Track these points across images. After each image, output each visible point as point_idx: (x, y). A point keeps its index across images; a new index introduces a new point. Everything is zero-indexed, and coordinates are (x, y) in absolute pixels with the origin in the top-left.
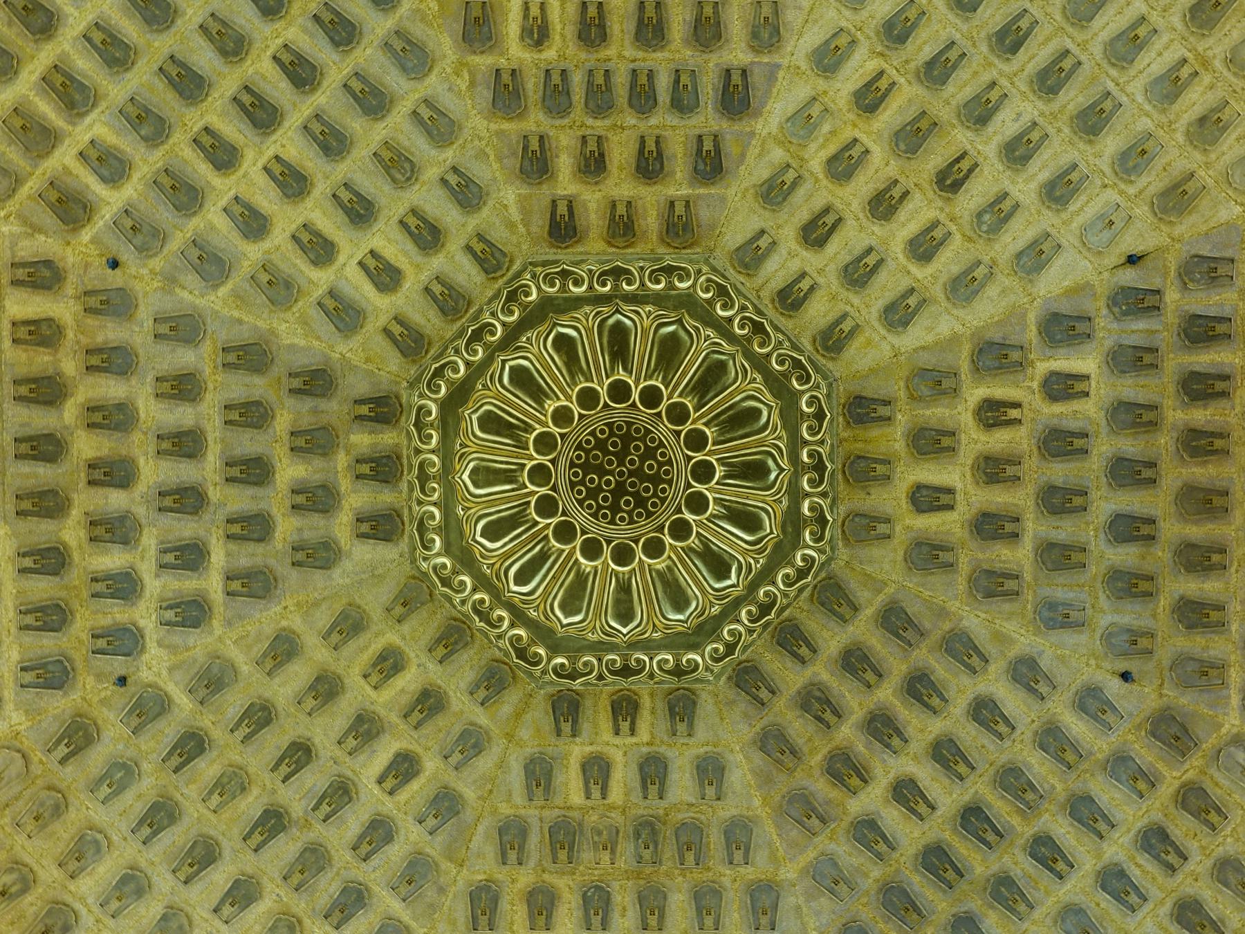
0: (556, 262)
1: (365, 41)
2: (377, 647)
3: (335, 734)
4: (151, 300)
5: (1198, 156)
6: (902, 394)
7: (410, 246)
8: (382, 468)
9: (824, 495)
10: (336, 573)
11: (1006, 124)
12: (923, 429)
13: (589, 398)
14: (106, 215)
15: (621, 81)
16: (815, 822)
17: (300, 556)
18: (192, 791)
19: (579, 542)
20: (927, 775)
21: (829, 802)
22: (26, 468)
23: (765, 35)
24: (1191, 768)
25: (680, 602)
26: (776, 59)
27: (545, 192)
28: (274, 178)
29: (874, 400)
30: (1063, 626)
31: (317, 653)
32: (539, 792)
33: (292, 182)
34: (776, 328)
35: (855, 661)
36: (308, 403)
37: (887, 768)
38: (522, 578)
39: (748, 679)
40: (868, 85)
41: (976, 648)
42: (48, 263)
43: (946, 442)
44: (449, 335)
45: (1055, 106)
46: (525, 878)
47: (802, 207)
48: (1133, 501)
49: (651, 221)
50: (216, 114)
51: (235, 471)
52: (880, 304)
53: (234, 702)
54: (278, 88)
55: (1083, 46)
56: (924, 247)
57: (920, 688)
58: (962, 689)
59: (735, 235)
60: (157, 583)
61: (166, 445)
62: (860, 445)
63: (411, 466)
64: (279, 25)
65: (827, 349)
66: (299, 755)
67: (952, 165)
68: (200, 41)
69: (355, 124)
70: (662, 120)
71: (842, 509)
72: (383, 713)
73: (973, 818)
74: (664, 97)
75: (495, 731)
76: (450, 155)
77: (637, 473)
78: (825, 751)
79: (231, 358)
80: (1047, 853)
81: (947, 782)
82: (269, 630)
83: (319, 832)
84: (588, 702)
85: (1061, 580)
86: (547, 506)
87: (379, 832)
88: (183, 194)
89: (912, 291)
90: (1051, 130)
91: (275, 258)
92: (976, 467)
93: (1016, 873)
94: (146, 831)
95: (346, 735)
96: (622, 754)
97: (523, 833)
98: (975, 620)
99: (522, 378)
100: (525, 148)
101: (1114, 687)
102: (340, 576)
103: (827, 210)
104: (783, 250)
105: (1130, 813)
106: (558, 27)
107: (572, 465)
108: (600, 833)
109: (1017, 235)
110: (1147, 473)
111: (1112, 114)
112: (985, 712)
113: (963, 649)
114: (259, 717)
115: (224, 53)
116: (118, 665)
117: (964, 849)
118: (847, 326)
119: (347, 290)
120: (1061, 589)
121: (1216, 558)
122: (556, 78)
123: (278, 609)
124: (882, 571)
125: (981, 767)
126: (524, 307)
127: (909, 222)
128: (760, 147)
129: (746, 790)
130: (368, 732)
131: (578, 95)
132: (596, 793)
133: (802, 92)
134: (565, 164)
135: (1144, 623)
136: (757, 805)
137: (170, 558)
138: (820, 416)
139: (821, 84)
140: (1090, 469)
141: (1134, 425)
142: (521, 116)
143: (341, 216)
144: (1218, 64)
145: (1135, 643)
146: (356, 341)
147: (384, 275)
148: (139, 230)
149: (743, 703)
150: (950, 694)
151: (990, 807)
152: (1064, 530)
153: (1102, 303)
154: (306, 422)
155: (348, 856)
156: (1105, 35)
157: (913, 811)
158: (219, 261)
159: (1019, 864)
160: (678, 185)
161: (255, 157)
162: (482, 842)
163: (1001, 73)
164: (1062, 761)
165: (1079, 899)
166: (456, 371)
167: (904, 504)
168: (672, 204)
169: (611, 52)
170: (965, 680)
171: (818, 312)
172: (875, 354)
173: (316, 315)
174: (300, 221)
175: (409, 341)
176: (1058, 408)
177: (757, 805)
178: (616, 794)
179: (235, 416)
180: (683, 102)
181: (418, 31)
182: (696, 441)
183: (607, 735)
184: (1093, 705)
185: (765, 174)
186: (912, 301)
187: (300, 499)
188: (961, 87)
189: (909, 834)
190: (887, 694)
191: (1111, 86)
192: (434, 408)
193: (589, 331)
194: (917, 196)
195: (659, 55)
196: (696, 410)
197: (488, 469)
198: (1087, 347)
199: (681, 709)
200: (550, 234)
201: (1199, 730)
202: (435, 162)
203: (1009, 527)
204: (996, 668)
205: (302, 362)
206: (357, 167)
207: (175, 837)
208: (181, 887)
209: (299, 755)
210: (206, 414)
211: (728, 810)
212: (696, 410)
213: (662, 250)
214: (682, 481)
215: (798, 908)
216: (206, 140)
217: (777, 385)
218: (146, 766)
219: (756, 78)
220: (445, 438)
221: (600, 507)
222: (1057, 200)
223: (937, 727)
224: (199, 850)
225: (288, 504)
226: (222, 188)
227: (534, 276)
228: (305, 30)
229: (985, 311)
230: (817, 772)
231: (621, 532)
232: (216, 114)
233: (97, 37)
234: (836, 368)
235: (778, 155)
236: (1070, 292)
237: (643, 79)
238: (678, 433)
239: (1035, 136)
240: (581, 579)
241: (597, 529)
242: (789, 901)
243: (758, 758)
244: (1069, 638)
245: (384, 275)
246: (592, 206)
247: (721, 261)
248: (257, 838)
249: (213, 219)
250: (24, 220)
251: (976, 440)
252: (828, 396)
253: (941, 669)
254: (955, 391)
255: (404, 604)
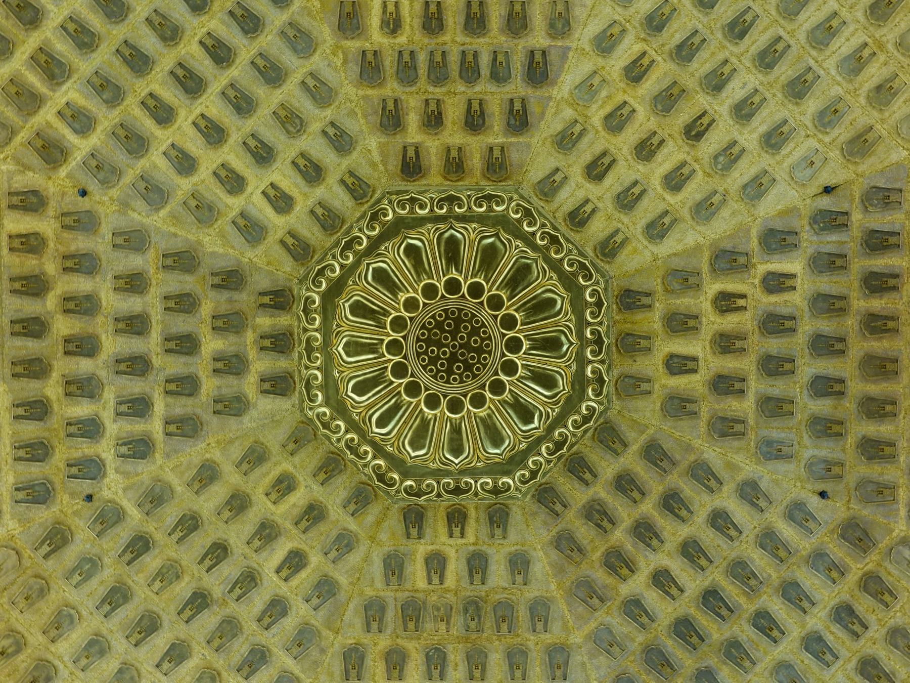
0: (406, 191)
1: (267, 30)
2: (275, 473)
3: (245, 537)
4: (110, 219)
5: (875, 114)
6: (659, 288)
7: (300, 180)
8: (279, 343)
9: (602, 362)
10: (246, 419)
11: (735, 91)
12: (674, 314)
13: (430, 291)
14: (77, 158)
15: (454, 59)
16: (595, 601)
17: (219, 407)
18: (141, 579)
19: (423, 396)
20: (677, 567)
21: (606, 587)
22: (19, 342)
23: (559, 26)
24: (870, 562)
25: (497, 440)
26: (567, 43)
27: (399, 140)
28: (200, 130)
29: (639, 293)
30: (777, 458)
31: (232, 478)
32: (394, 579)
33: (213, 133)
34: (568, 240)
35: (625, 484)
36: (225, 295)
37: (648, 562)
38: (381, 423)
39: (546, 496)
40: (634, 62)
41: (713, 474)
42: (35, 193)
43: (691, 323)
44: (328, 245)
45: (771, 77)
46: (384, 642)
47: (586, 151)
48: (828, 367)
49: (476, 162)
50: (158, 83)
51: (172, 345)
52: (643, 222)
53: (171, 514)
54: (203, 64)
55: (792, 33)
56: (675, 181)
57: (672, 503)
58: (703, 504)
59: (537, 172)
60: (115, 426)
61: (121, 326)
62: (628, 326)
63: (300, 341)
64: (204, 18)
65: (604, 255)
66: (219, 552)
67: (696, 120)
68: (146, 30)
69: (260, 91)
70: (484, 88)
71: (616, 372)
72: (280, 521)
73: (711, 598)
74: (485, 71)
75: (362, 534)
76: (329, 113)
77: (466, 346)
78: (603, 549)
79: (169, 262)
80: (765, 624)
81: (692, 572)
82: (197, 461)
83: (233, 608)
84: (430, 513)
85: (775, 424)
86: (400, 370)
87: (277, 609)
88: (134, 142)
89: (666, 212)
90: (768, 95)
91: (201, 189)
92: (713, 342)
93: (743, 638)
94: (107, 608)
95: (253, 537)
96: (455, 551)
97: (383, 609)
98: (713, 453)
99: (381, 277)
100: (384, 108)
101: (814, 502)
102: (248, 421)
103: (604, 154)
104: (572, 183)
105: (826, 594)
106: (408, 20)
107: (418, 340)
108: (438, 609)
109: (744, 172)
110: (838, 346)
111: (813, 83)
112: (720, 521)
113: (704, 475)
114: (190, 524)
115: (164, 39)
116: (86, 486)
117: (704, 621)
118: (619, 238)
119: (253, 212)
120: (776, 431)
121: (888, 408)
122: (406, 57)
123: (203, 445)
124: (645, 417)
125: (717, 561)
126: (383, 224)
127: (664, 162)
128: (556, 108)
129: (545, 578)
130: (269, 535)
131: (423, 69)
132: (436, 580)
133: (586, 67)
134: (413, 120)
135: (836, 455)
136: (553, 589)
137: (124, 408)
138: (599, 304)
139: (600, 61)
140: (797, 343)
141: (829, 311)
142: (381, 85)
143: (249, 158)
144: (890, 47)
145: (829, 470)
146: (261, 249)
147: (281, 201)
148: (101, 169)
149: (543, 514)
150: (695, 508)
151: (723, 590)
152: (778, 388)
153: (805, 222)
154: (224, 309)
155: (254, 626)
156: (808, 26)
157: (667, 593)
158: (160, 191)
159: (745, 632)
160: (496, 136)
161: (187, 115)
162: (353, 616)
163: (732, 54)
164: (776, 556)
165: (789, 657)
166: (333, 271)
167: (661, 368)
168: (491, 149)
169: (447, 38)
170: (706, 497)
171: (598, 228)
172: (639, 259)
173: (231, 230)
174: (219, 161)
175: (299, 250)
176: (773, 298)
177: (553, 589)
178: (450, 580)
179: (171, 304)
180: (499, 75)
181: (305, 22)
182: (509, 323)
183: (443, 537)
184: (799, 515)
185: (560, 127)
186: (667, 220)
187: (219, 365)
188: (703, 64)
189: (665, 610)
190: (648, 507)
191: (812, 63)
192: (317, 298)
193: (431, 242)
194: (670, 143)
195: (482, 40)
196: (509, 299)
197: (357, 343)
198: (795, 254)
199: (498, 518)
200: (402, 171)
201: (876, 534)
202: (318, 118)
203: (738, 386)
204: (728, 488)
205: (221, 264)
206: (261, 122)
207: (128, 612)
208: (133, 648)
209: (219, 552)
210: (151, 303)
211: (532, 592)
212: (509, 299)
213: (484, 183)
214: (498, 352)
215: (583, 664)
216: (151, 103)
217: (568, 281)
218: (107, 560)
219: (553, 57)
220: (326, 320)
221: (438, 371)
222: (773, 146)
223: (685, 531)
224: (146, 622)
225: (210, 368)
226: (162, 138)
227: (390, 202)
228: (223, 22)
229: (720, 228)
230: (597, 565)
231: (454, 389)
232: (158, 83)
233: (71, 27)
234: (611, 269)
235: (569, 113)
236: (782, 214)
237: (470, 58)
238: (496, 317)
239: (756, 99)
240: (425, 424)
241: (436, 387)
242: (577, 659)
243: (554, 554)
244: (782, 466)
245: (281, 201)
246: (433, 151)
247: (527, 191)
248: (188, 613)
249: (156, 160)
250: (17, 161)
251: (714, 322)
252: (606, 289)
253: (688, 489)
254: (698, 286)
255: (296, 442)
